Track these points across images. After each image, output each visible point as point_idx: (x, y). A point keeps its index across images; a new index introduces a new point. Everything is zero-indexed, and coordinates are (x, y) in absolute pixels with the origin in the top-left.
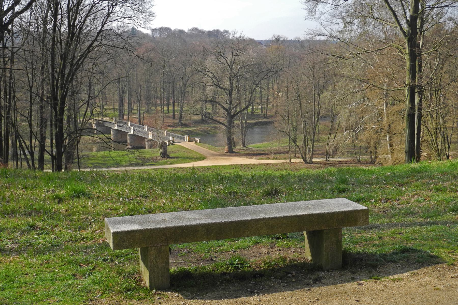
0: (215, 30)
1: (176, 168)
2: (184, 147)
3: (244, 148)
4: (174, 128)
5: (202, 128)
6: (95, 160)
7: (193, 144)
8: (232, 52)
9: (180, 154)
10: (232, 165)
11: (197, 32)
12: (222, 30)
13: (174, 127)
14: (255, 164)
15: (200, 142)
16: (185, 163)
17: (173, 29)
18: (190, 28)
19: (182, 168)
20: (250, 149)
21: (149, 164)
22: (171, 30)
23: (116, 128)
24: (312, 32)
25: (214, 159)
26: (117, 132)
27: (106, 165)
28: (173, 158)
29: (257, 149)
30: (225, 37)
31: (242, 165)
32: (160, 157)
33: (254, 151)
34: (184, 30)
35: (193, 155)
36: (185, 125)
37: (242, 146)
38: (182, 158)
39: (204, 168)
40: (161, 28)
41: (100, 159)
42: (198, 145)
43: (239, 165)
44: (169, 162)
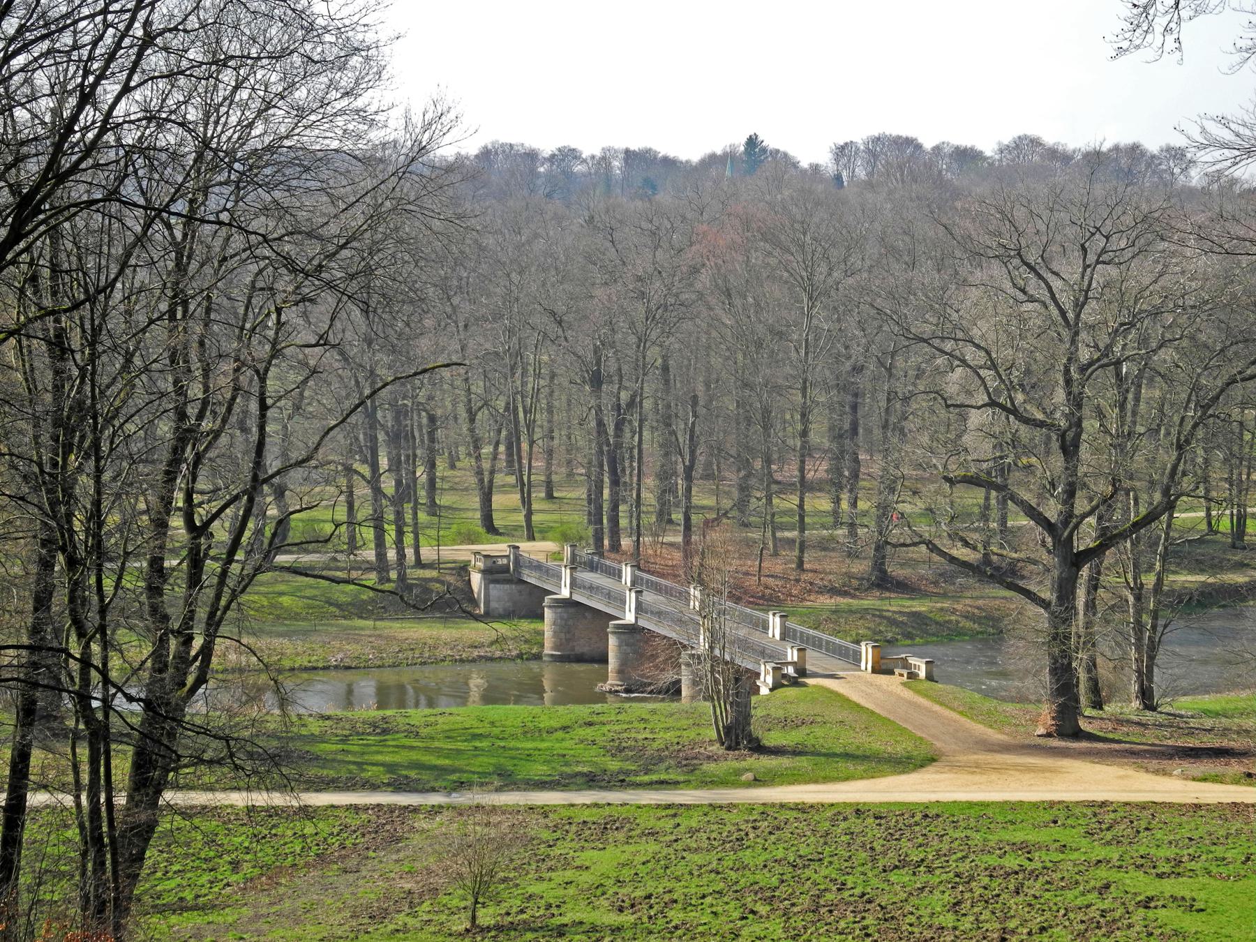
0: (1122, 145)
1: (773, 805)
2: (848, 700)
3: (1149, 716)
4: (843, 601)
5: (980, 602)
6: (412, 748)
7: (893, 683)
8: (1083, 246)
9: (817, 736)
10: (1052, 804)
11: (1036, 158)
12: (1153, 145)
13: (845, 594)
14: (1170, 805)
15: (930, 677)
16: (826, 780)
17: (928, 144)
18: (1007, 140)
19: (802, 808)
20: (1175, 722)
21: (655, 777)
22: (918, 147)
23: (565, 593)
24: (1227, 136)
25: (977, 768)
26: (572, 610)
27: (454, 777)
28: (777, 751)
29: (1208, 723)
30: (1167, 176)
31: (1103, 804)
32: (716, 748)
33: (1191, 732)
34: (979, 147)
35: (878, 743)
36: (902, 587)
37: (1136, 704)
38: (819, 754)
39: (906, 810)
40: (877, 140)
41: (437, 744)
42: (918, 692)
43: (1091, 804)
44: (748, 776)
